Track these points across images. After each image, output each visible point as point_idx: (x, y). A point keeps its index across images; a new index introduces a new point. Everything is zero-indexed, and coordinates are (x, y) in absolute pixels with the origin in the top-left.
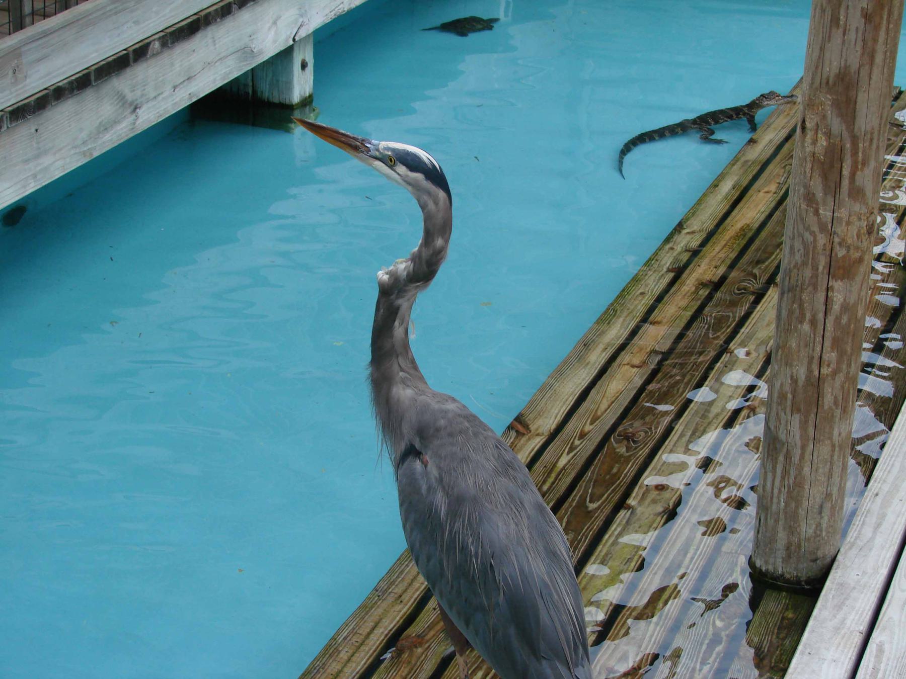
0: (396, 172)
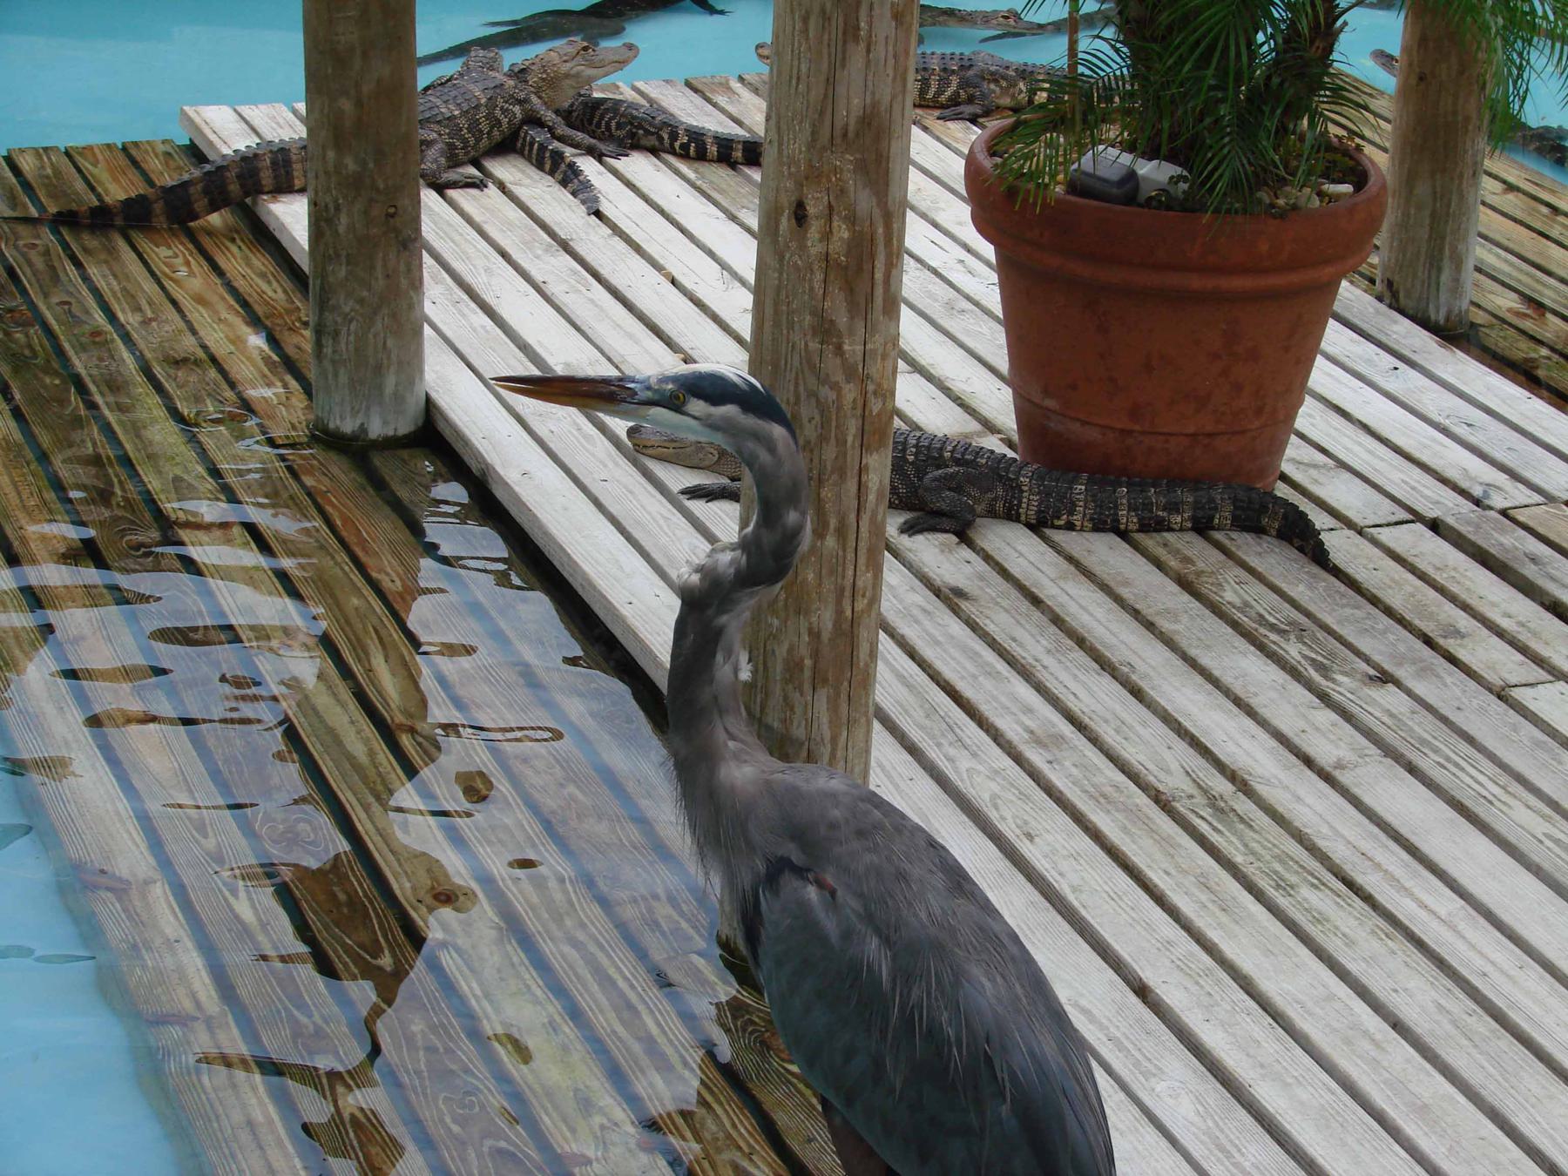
0: (689, 415)
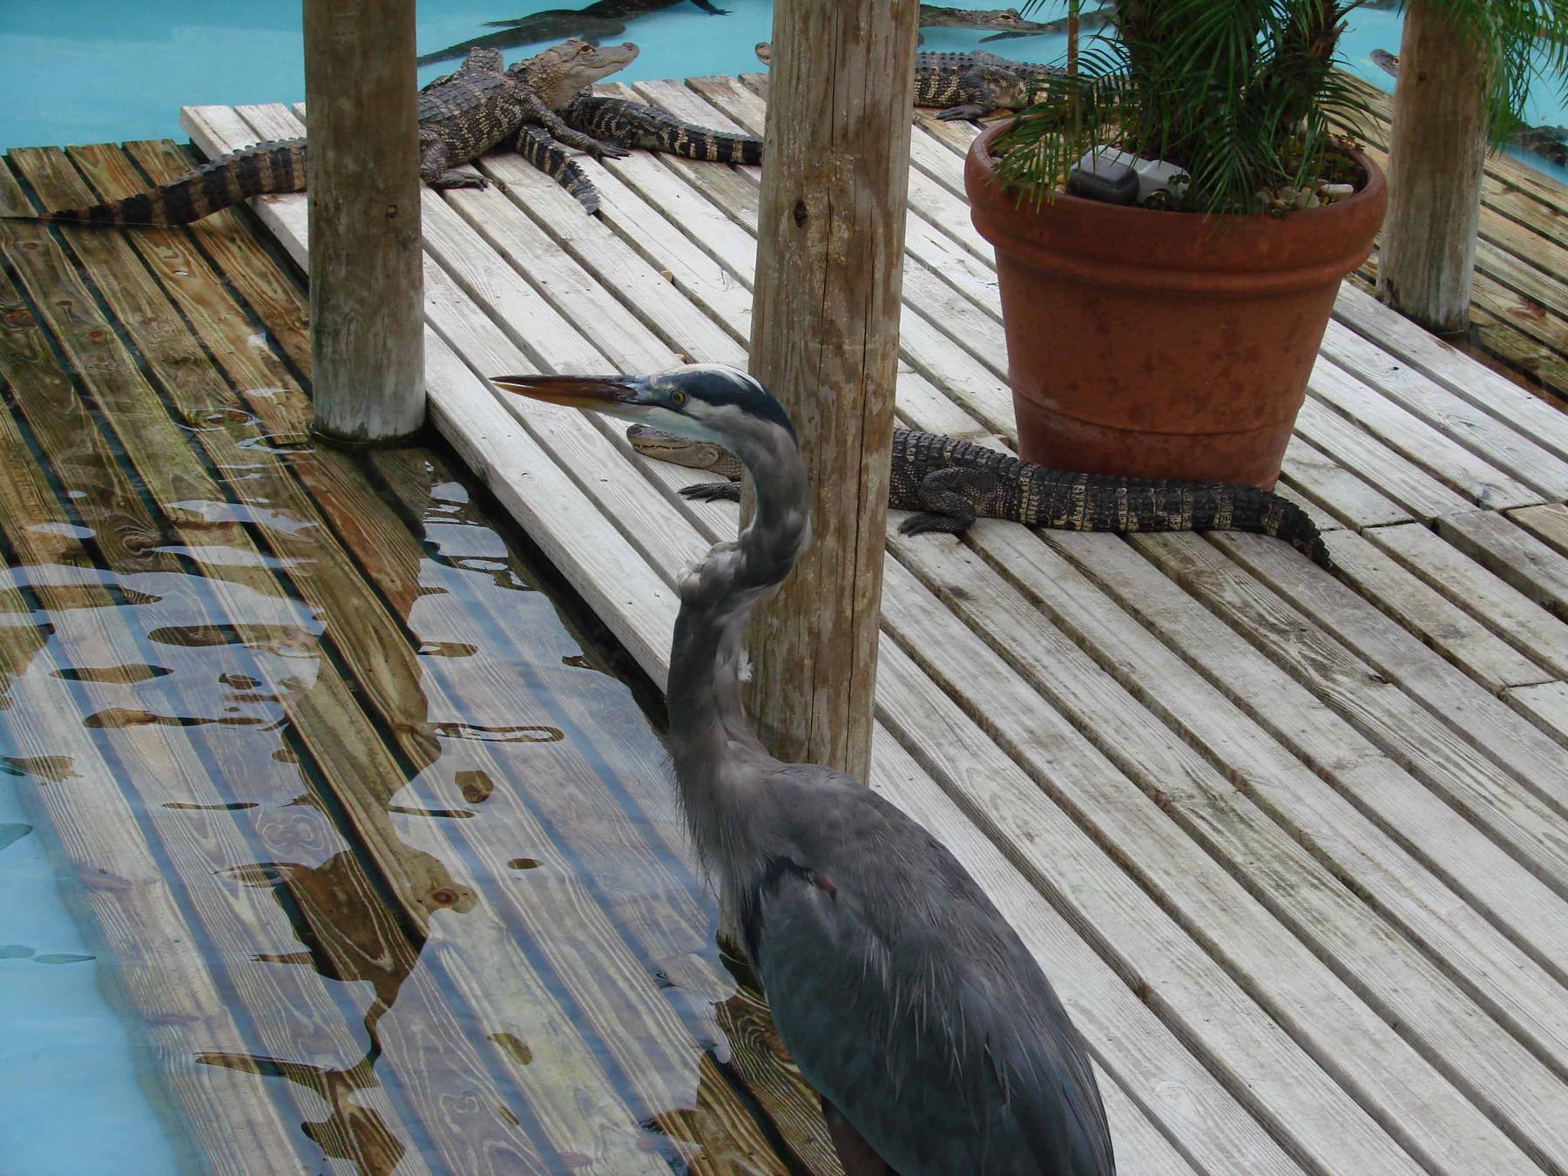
0: (689, 415)
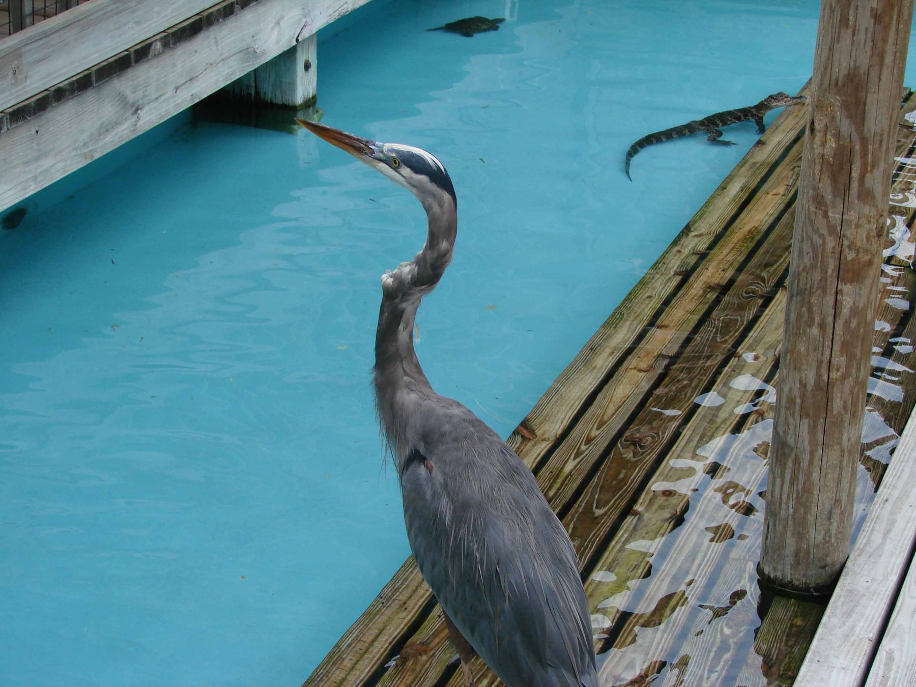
0: (400, 174)
